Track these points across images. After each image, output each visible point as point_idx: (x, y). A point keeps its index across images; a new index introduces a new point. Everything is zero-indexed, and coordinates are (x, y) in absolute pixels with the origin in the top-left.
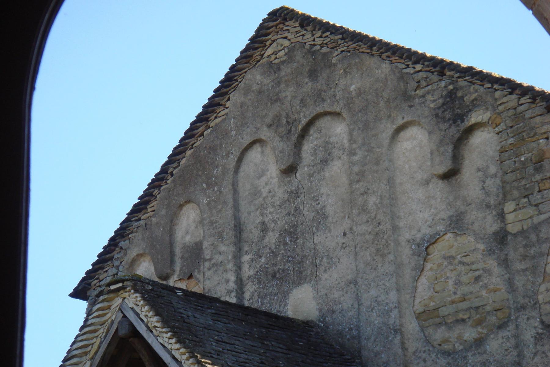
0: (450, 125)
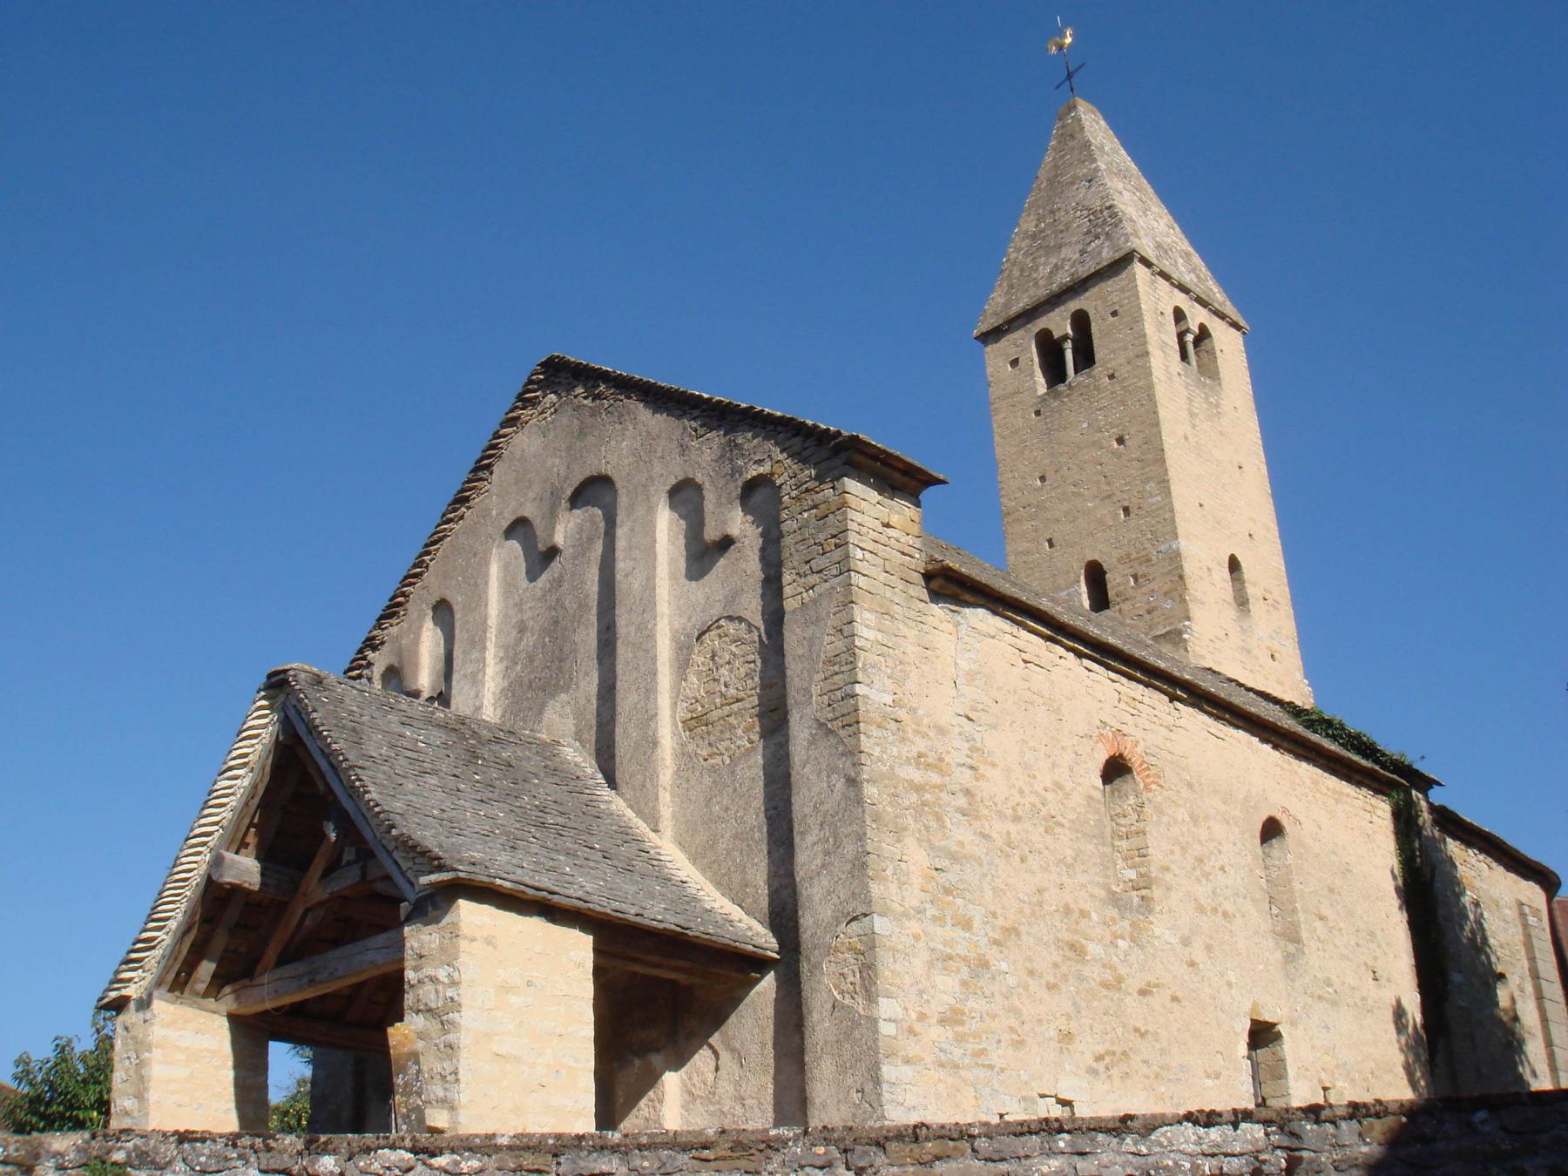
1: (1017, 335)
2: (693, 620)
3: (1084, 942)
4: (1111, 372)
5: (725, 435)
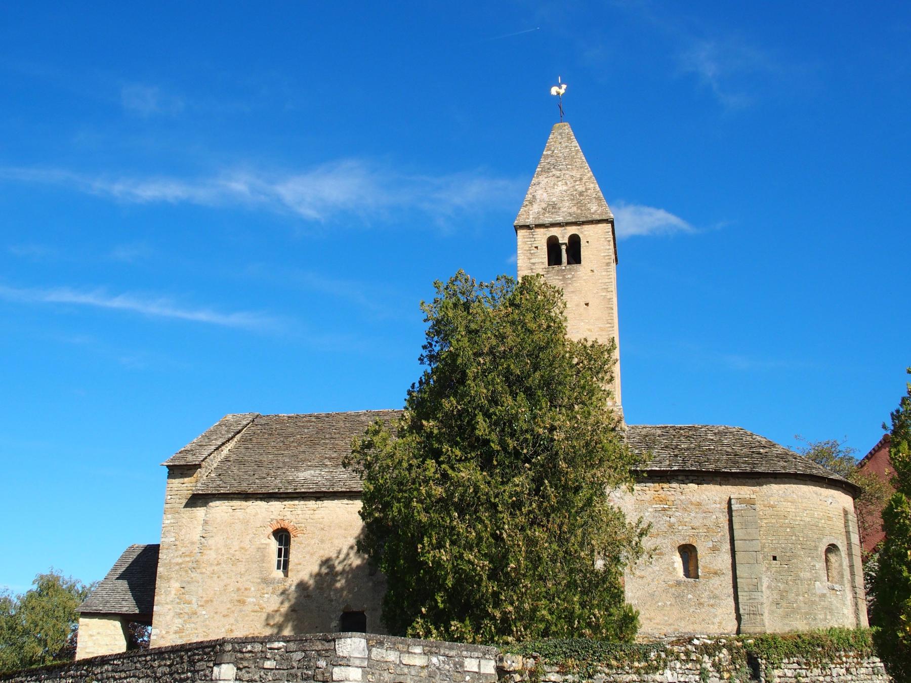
3: (245, 598)
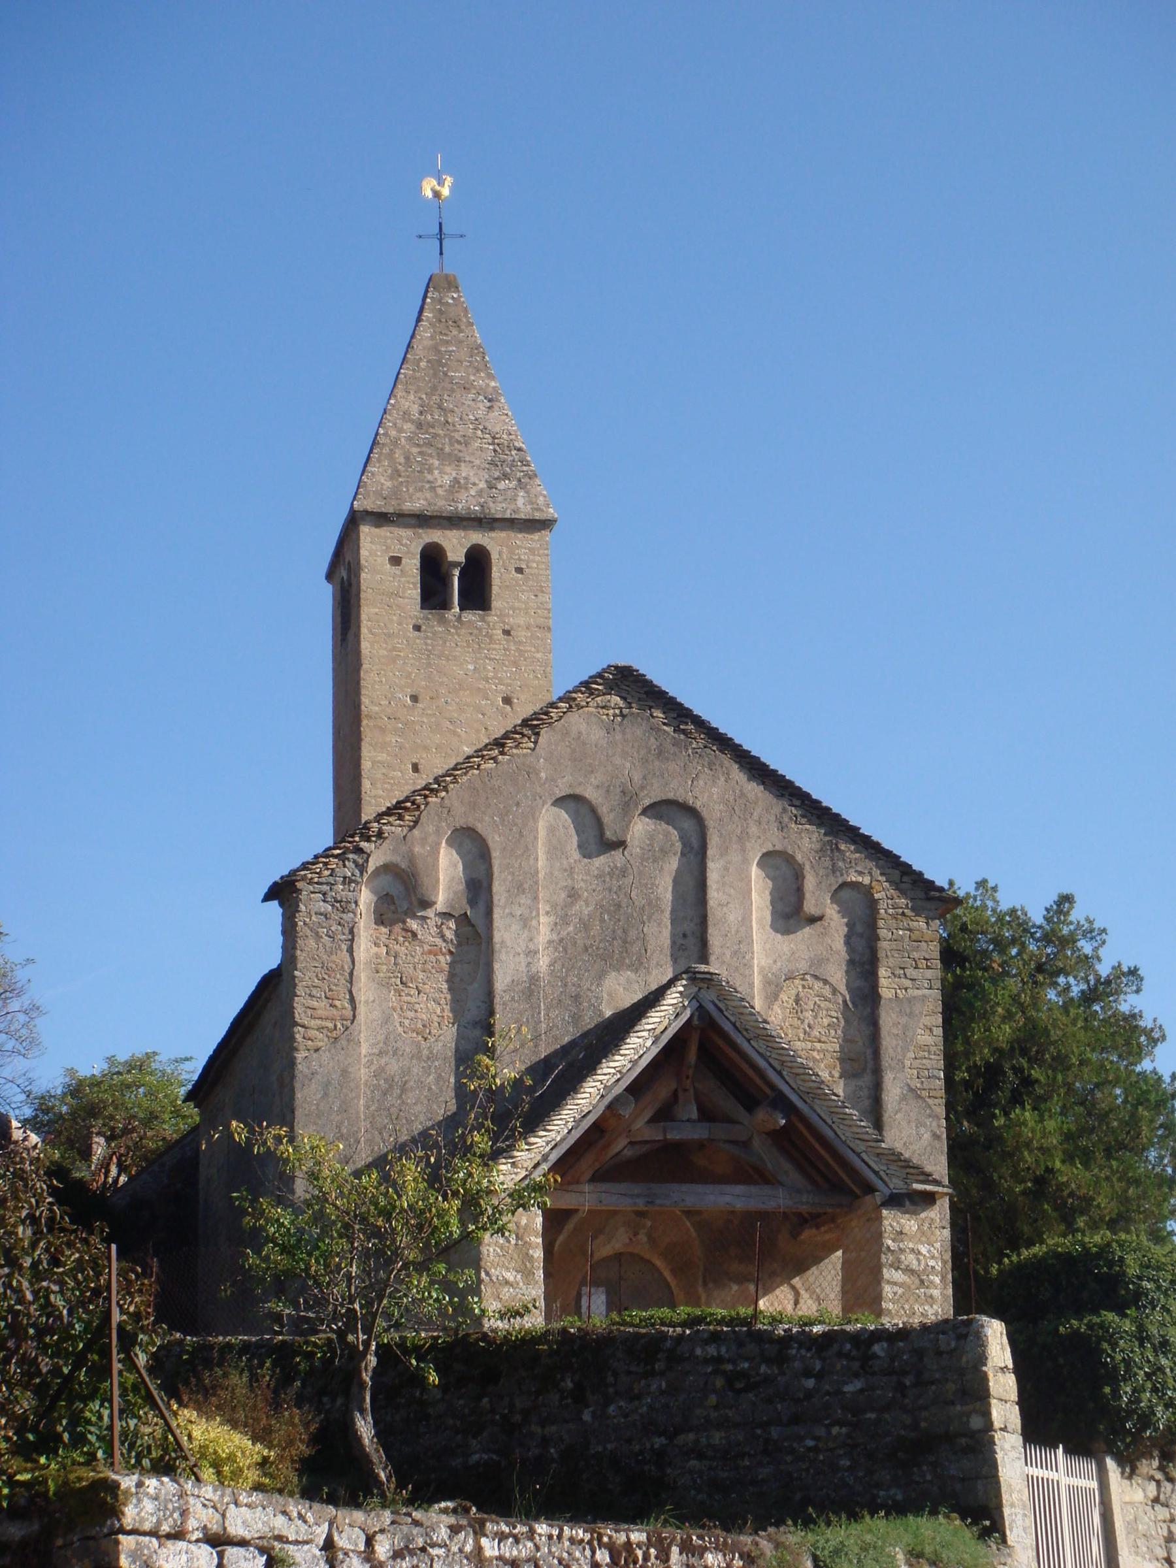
0: (827, 876)
1: (405, 533)
2: (779, 964)
4: (507, 627)
5: (825, 834)
